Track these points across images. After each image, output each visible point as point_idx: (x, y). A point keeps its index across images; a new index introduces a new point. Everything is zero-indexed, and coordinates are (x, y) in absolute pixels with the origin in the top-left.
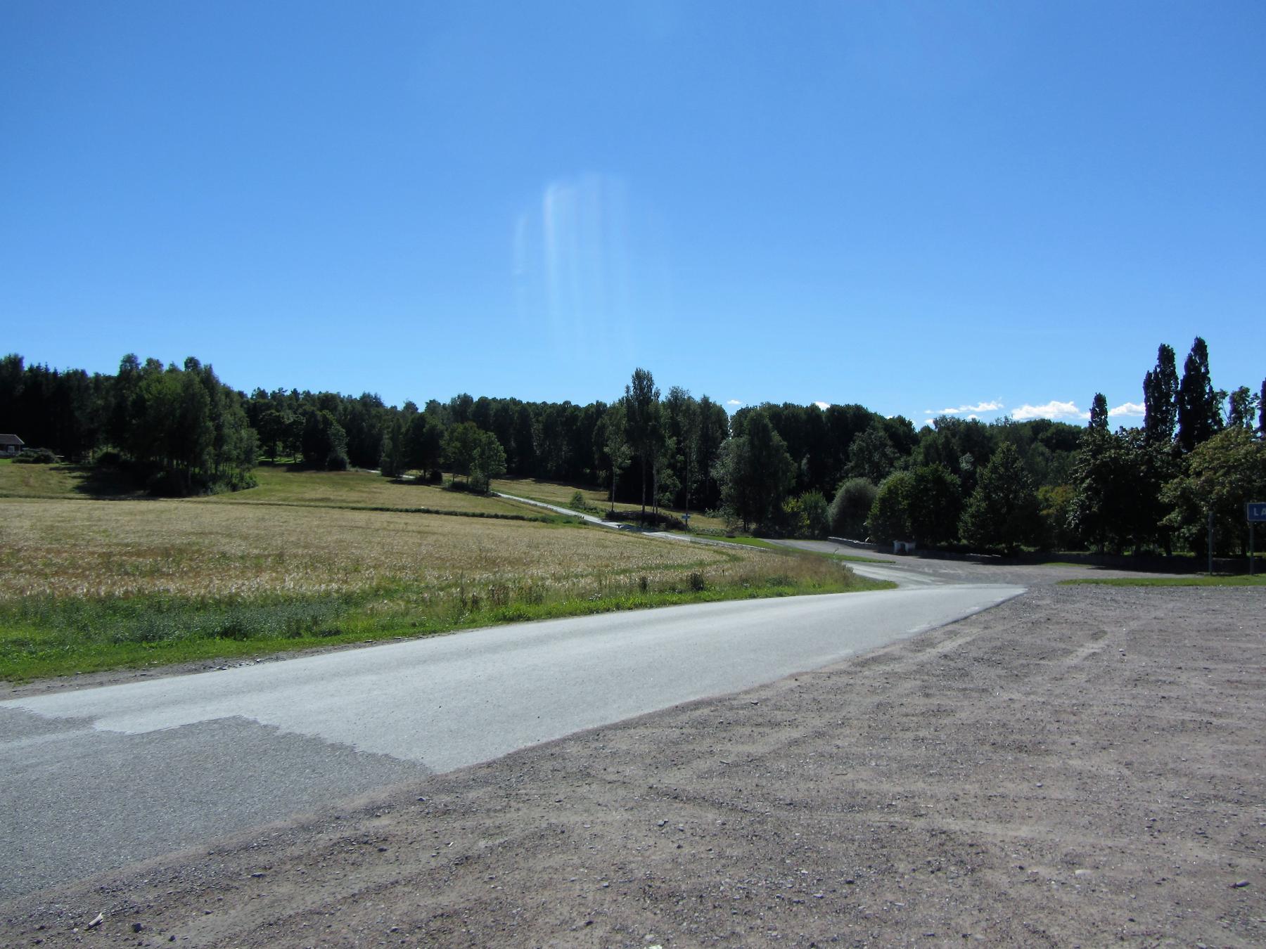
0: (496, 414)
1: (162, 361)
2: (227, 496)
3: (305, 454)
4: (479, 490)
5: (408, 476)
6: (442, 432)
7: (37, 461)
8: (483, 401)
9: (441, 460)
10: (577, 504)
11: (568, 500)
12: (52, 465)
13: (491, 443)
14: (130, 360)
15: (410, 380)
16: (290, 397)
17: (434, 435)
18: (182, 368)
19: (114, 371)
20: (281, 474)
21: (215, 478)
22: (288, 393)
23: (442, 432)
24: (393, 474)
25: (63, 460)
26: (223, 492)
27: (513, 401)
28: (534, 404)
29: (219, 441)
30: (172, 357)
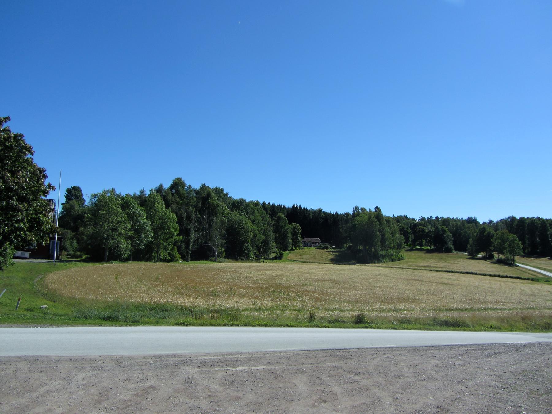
0: (528, 225)
1: (366, 208)
2: (391, 264)
3: (435, 246)
5: (480, 256)
6: (493, 235)
7: (324, 248)
8: (522, 220)
9: (492, 248)
15: (489, 211)
16: (435, 220)
17: (490, 236)
20: (422, 254)
21: (384, 257)
22: (434, 218)
23: (493, 235)
24: (472, 256)
25: (336, 248)
26: (387, 262)
27: (539, 218)
29: (383, 240)
30: (370, 207)
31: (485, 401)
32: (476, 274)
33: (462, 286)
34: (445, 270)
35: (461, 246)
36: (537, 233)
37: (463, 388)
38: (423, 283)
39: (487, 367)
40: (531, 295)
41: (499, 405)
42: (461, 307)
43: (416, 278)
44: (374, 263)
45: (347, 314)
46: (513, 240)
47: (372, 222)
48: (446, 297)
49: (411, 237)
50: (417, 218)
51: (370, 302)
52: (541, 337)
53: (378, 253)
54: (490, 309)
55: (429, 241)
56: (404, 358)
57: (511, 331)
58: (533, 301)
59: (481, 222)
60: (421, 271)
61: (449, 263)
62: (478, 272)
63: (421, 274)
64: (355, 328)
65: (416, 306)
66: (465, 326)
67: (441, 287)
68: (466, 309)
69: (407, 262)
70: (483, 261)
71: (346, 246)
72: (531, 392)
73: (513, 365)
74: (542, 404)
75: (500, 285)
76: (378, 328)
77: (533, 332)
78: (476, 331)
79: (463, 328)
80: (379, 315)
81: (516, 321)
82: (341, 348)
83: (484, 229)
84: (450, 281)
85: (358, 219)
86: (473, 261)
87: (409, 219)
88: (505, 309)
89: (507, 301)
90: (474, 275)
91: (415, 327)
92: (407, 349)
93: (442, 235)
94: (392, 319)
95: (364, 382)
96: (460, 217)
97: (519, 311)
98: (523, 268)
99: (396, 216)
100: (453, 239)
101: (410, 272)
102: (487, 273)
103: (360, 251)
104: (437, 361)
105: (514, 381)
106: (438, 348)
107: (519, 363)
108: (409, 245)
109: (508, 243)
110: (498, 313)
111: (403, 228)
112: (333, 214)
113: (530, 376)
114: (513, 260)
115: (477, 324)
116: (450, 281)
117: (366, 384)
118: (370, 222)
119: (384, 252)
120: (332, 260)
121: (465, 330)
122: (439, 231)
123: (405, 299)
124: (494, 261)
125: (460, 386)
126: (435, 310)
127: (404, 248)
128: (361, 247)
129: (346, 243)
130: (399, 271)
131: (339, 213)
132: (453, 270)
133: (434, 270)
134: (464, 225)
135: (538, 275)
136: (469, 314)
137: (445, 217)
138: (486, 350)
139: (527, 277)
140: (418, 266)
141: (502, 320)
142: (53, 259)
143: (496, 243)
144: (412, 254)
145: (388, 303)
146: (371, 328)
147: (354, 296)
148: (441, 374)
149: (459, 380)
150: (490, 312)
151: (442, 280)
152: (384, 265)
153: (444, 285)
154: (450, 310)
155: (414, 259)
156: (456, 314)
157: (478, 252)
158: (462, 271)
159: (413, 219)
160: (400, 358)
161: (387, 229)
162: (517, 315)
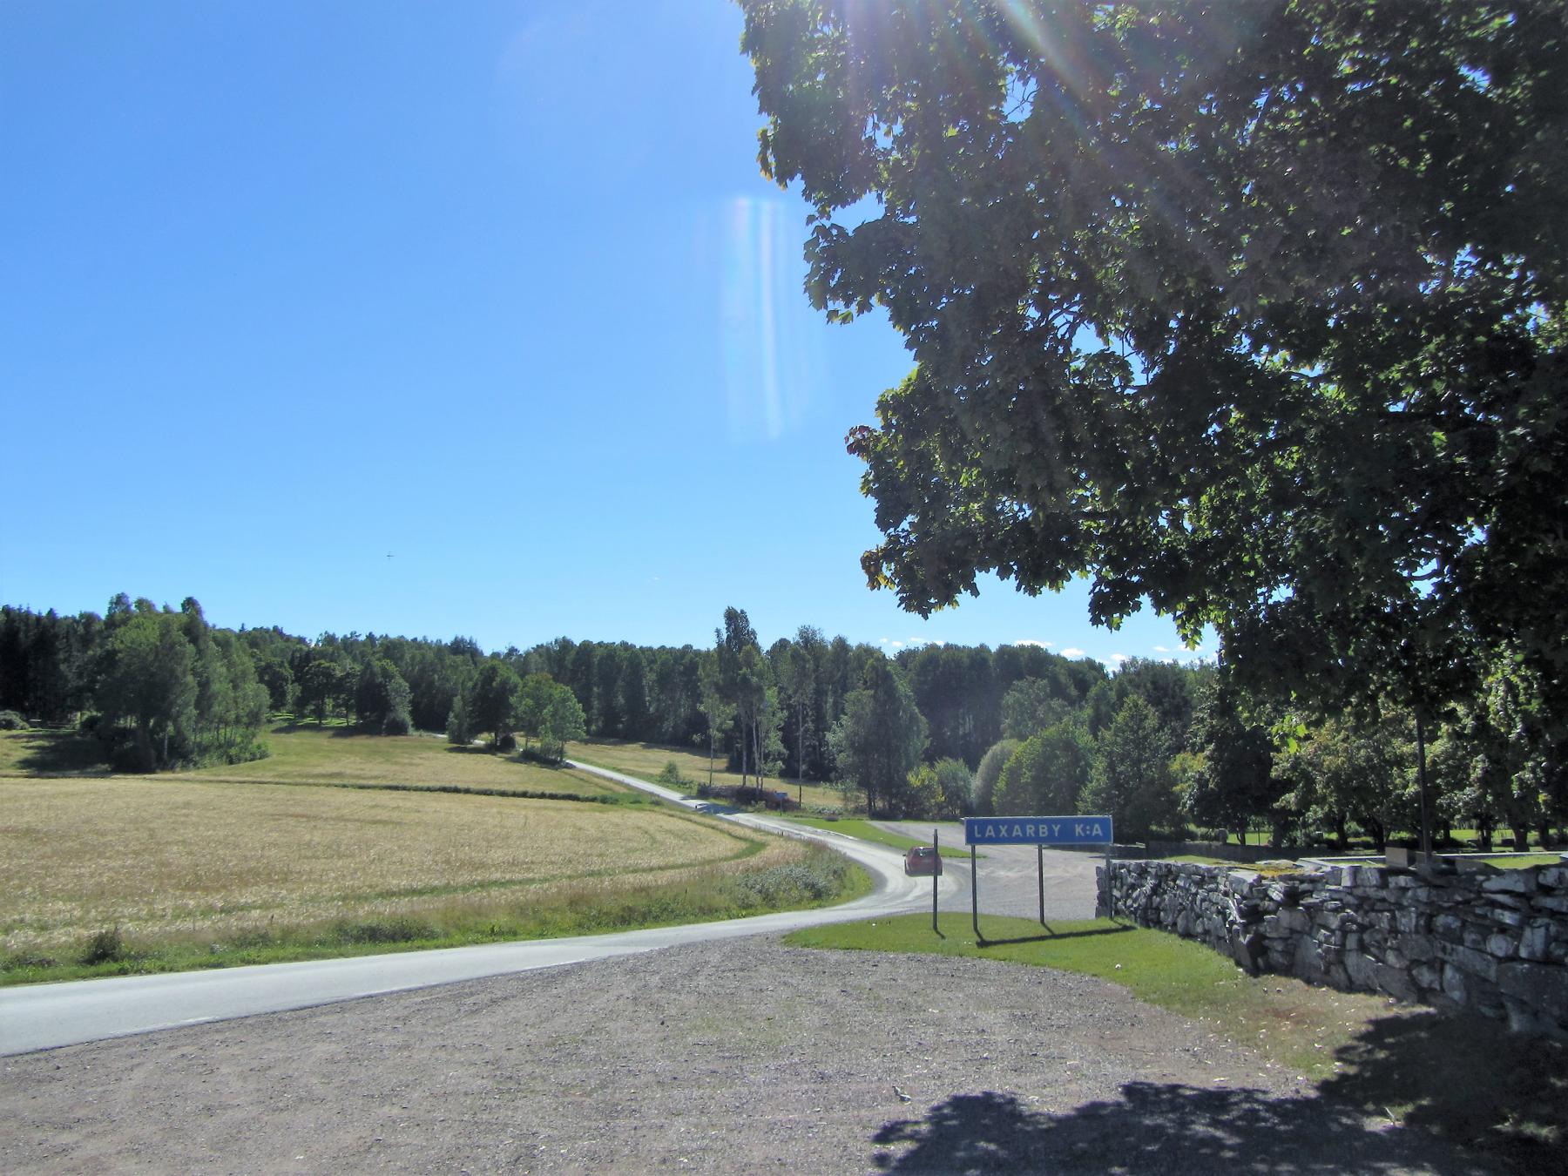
2: (225, 772)
3: (360, 714)
4: (548, 760)
5: (479, 742)
8: (586, 646)
9: (511, 722)
10: (670, 777)
11: (658, 771)
12: (14, 732)
13: (564, 700)
14: (120, 600)
16: (364, 643)
17: (506, 690)
18: (179, 609)
19: (706, 641)
20: (322, 740)
21: (204, 750)
22: (363, 638)
23: (516, 686)
24: (460, 744)
25: (41, 725)
26: (213, 765)
27: (625, 645)
28: (650, 649)
29: (204, 702)
30: (168, 598)
31: (448, 1137)
32: (467, 791)
33: (427, 825)
34: (385, 783)
35: (430, 717)
36: (620, 683)
37: (396, 1111)
38: (320, 823)
39: (467, 1041)
40: (598, 840)
41: (482, 1142)
42: (420, 885)
43: (299, 810)
44: (172, 769)
45: (61, 936)
46: (564, 700)
47: (172, 646)
48: (381, 860)
49: (293, 691)
50: (313, 637)
51: (147, 892)
52: (609, 945)
53: (185, 739)
54: (495, 883)
55: (346, 704)
56: (235, 1050)
57: (542, 936)
58: (601, 855)
59: (487, 653)
60: (315, 789)
61: (396, 763)
62: (473, 786)
63: (316, 797)
64: (84, 978)
65: (292, 891)
66: (423, 937)
67: (371, 832)
68: (433, 890)
69: (276, 763)
70: (487, 757)
71: (78, 718)
72: (566, 1089)
73: (533, 1026)
74: (588, 1118)
75: (526, 817)
76: (163, 970)
77: (595, 933)
78: (452, 946)
79: (417, 943)
80: (173, 928)
81: (555, 910)
82: (23, 1050)
83: (494, 669)
84: (395, 814)
85: (122, 640)
86: (460, 757)
87: (288, 639)
88: (532, 881)
89: (541, 858)
90: (461, 796)
91: (281, 953)
92: (249, 1021)
93: (382, 686)
94: (212, 937)
95: (91, 1148)
96: (432, 638)
97: (565, 882)
98: (582, 771)
99: (249, 628)
100: (411, 696)
101: (281, 793)
102: (496, 788)
103: (125, 733)
104: (333, 1047)
105: (528, 1068)
106: (341, 1006)
107: (547, 1019)
108: (284, 715)
109: (550, 708)
110: (513, 893)
111: (269, 666)
112: (39, 619)
113: (571, 1048)
114: (561, 752)
115: (457, 927)
116: (395, 814)
117: (94, 1153)
118: (167, 649)
119: (206, 737)
120: (26, 764)
121: (423, 948)
122: (373, 674)
123: (259, 874)
124: (514, 754)
125: (386, 1109)
126: (344, 899)
127: (270, 721)
128: (130, 722)
129: (80, 709)
130: (248, 792)
131: (61, 613)
132: (407, 784)
133: (353, 786)
134: (442, 660)
135: (617, 788)
136: (439, 902)
137: (393, 635)
138: (472, 994)
139: (590, 795)
140: (308, 776)
141: (521, 909)
142: (1115, 841)
143: (521, 709)
144: (293, 739)
145: (206, 889)
146: (138, 972)
147: (92, 876)
148: (336, 1082)
149: (386, 1091)
150: (494, 892)
151: (373, 812)
152: (203, 774)
153: (380, 828)
154: (388, 894)
155: (297, 754)
156: (403, 906)
157: (475, 731)
158: (431, 784)
159: (301, 640)
160: (220, 1052)
161: (219, 668)
162: (559, 893)
